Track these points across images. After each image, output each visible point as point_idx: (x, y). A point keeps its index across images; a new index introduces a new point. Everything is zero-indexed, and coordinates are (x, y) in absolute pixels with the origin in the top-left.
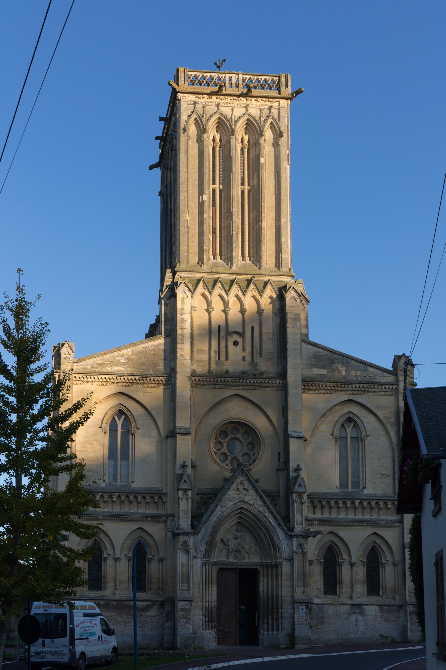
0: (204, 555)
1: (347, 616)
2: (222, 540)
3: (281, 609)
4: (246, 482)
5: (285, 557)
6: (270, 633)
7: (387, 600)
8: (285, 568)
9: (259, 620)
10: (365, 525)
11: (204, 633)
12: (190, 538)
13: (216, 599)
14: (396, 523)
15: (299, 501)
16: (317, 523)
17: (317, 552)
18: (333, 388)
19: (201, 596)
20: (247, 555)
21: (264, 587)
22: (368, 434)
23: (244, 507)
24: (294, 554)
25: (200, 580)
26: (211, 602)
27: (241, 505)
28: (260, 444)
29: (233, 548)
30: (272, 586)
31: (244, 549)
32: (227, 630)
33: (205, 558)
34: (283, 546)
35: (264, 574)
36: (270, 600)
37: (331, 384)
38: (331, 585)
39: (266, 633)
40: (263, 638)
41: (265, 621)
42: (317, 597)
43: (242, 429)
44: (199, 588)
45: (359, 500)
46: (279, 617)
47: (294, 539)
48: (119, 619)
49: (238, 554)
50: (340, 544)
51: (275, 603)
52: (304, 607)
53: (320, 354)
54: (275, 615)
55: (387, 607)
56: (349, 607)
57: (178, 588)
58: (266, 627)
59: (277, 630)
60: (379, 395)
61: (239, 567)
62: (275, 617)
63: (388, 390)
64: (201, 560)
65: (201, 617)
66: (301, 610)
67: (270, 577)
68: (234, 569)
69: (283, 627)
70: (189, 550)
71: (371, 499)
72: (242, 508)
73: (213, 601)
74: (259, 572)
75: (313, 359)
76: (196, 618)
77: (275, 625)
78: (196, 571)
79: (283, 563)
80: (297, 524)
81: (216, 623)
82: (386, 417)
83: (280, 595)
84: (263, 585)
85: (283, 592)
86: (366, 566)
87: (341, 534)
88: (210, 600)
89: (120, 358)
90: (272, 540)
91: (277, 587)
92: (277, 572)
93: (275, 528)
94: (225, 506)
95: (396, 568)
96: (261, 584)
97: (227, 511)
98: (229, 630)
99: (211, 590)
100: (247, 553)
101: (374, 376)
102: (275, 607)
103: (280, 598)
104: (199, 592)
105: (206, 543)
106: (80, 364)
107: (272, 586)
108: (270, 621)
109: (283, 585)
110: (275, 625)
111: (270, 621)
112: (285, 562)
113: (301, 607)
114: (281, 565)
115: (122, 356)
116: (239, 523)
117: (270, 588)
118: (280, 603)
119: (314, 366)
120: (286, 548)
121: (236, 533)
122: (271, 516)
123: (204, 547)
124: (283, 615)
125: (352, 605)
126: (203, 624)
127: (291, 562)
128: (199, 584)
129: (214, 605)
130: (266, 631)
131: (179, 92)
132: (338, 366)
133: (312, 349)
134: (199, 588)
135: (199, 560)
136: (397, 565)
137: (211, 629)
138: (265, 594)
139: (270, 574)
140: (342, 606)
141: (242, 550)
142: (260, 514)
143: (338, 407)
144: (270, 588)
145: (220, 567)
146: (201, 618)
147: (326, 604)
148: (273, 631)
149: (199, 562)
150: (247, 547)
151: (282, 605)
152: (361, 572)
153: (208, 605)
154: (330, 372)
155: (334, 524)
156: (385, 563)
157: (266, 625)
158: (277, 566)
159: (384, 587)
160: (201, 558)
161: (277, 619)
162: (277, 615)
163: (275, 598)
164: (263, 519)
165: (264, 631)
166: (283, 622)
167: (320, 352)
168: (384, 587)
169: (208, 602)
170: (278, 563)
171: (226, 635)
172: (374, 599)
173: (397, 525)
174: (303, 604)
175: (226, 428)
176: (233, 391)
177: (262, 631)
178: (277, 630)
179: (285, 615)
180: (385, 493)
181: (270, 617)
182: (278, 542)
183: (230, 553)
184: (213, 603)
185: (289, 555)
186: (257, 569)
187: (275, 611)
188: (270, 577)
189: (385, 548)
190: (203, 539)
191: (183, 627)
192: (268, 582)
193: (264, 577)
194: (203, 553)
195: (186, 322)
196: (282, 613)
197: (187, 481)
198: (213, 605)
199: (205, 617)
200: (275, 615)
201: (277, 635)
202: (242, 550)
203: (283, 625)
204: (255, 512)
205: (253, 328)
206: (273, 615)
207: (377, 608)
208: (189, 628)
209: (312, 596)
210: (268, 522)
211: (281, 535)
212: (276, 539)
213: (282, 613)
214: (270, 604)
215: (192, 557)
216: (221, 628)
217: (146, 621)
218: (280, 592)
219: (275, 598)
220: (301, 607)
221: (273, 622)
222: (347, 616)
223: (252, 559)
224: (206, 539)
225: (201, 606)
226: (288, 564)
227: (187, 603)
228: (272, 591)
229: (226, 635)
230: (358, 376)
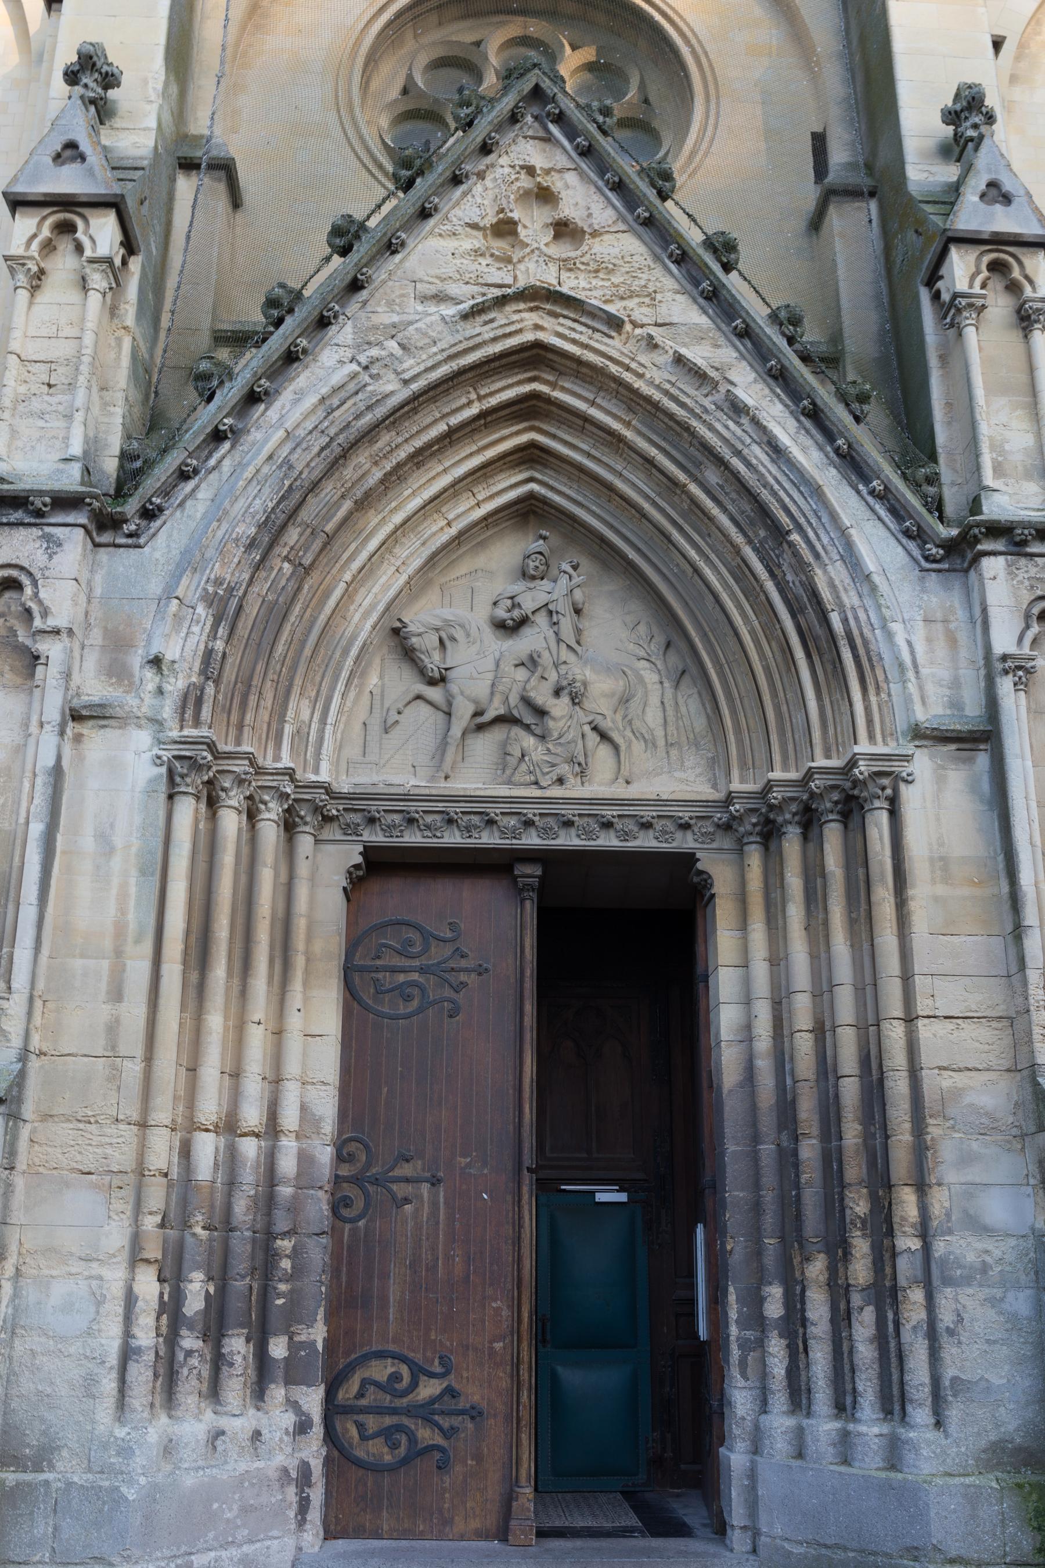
0: (191, 703)
2: (399, 640)
3: (921, 1187)
4: (571, 178)
5: (921, 715)
6: (824, 1427)
8: (936, 806)
9: (717, 1298)
11: (126, 1451)
12: (52, 545)
13: (326, 1105)
15: (999, 306)
19: (134, 1069)
20: (604, 752)
21: (747, 1001)
24: (1005, 686)
25: (138, 917)
26: (272, 1129)
27: (530, 325)
28: (687, 76)
29: (481, 689)
30: (823, 990)
31: (576, 700)
32: (429, 1389)
33: (197, 723)
34: (896, 627)
35: (742, 899)
36: (807, 1108)
39: (780, 1422)
40: (752, 1474)
41: (774, 1308)
43: (574, 48)
44: (117, 994)
46: (904, 1265)
47: (993, 567)
49: (529, 742)
51: (852, 1133)
54: (861, 1246)
58: (778, 1367)
59: (894, 1402)
61: (532, 840)
62: (860, 1271)
65: (115, 1276)
67: (795, 912)
68: (493, 865)
69: (949, 1372)
70: (45, 647)
72: (535, 356)
73: (290, 1118)
74: (706, 881)
76: (59, 1290)
77: (865, 1352)
78: (103, 838)
79: (903, 769)
80: (999, 470)
81: (318, 1334)
83: (896, 1058)
84: (746, 985)
85: (925, 1030)
88: (252, 1115)
90: (809, 605)
91: (868, 987)
92: (857, 858)
93: (817, 492)
96: (725, 983)
97: (411, 365)
98: (451, 1392)
99: (279, 1033)
100: (604, 736)
102: (854, 1170)
103: (898, 1086)
104: (113, 1029)
105: (209, 600)
107: (823, 990)
108: (818, 1308)
109: (920, 964)
110: (865, 1352)
111: (818, 1308)
112: (923, 764)
114: (890, 783)
116: (527, 512)
117: (802, 1005)
118: (902, 1135)
120: (920, 648)
121: (519, 587)
123: (198, 636)
124: (939, 1248)
126: (127, 1354)
127: (983, 760)
128: (118, 953)
129: (305, 1159)
130: (779, 1400)
134: (117, 994)
135: (142, 738)
137: (259, 1392)
138: (764, 1065)
139: (794, 882)
141: (559, 707)
142: (693, 394)
144: (802, 1005)
145: (376, 837)
146: (116, 1289)
148: (844, 1405)
149: (126, 765)
150: (602, 689)
151: (921, 1148)
153: (231, 1159)
157: (776, 1347)
158: (852, 800)
160: (157, 723)
161: (886, 1294)
162: (884, 1254)
163: (850, 1090)
164: (719, 431)
165: (764, 1406)
166: (946, 1318)
169: (229, 1126)
170: (863, 769)
171: (426, 1435)
177: (741, 1399)
178: (894, 1402)
179: (956, 1247)
181: (817, 1269)
182: (850, 599)
183: (456, 731)
184: (289, 1146)
185: (956, 704)
186: (688, 859)
187: (859, 1206)
188: (795, 912)
190: (189, 562)
192: (778, 960)
193: (743, 926)
194: (176, 685)
196: (924, 1233)
197: (85, 146)
198: (287, 1165)
199: (172, 1276)
200: (861, 1246)
201: (894, 1454)
202: (559, 707)
203: (950, 1352)
204: (652, 375)
206: (839, 1251)
210: (758, 454)
211: (878, 546)
212: (830, 577)
213: (924, 1233)
214: (809, 1150)
215: (53, 707)
216: (381, 1371)
218: (895, 1033)
219: (850, 1090)
221: (841, 1319)
223: (643, 764)
224: (218, 570)
225: (123, 1157)
226: (957, 778)
228: (823, 1030)
229: (426, 1435)
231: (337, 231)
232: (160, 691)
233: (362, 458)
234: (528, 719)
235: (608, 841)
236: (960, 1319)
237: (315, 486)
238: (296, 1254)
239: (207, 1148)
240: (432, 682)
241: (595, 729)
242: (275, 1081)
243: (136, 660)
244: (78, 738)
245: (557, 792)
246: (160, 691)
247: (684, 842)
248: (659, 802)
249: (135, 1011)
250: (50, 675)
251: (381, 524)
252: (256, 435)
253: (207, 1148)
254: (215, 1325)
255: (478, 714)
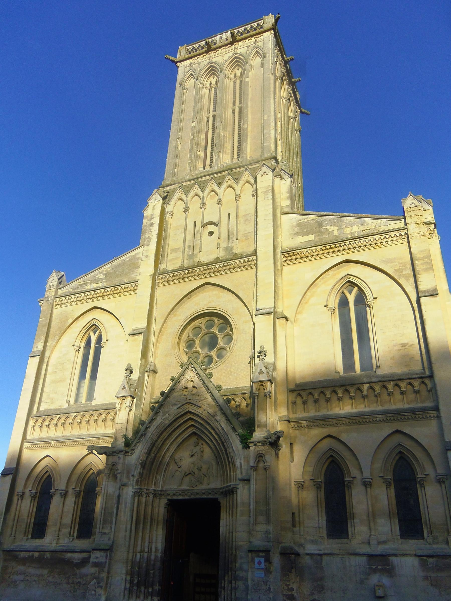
1: (363, 577)
7: (435, 546)
10: (380, 420)
14: (429, 412)
16: (305, 425)
17: (310, 469)
18: (322, 252)
19: (127, 543)
22: (374, 297)
23: (191, 411)
25: (129, 518)
37: (318, 248)
38: (338, 520)
42: (313, 542)
45: (368, 385)
48: (50, 579)
50: (346, 454)
52: (262, 560)
53: (305, 220)
55: (434, 559)
56: (365, 558)
57: (97, 530)
60: (384, 247)
63: (395, 238)
64: (133, 489)
65: (124, 577)
66: (257, 565)
71: (386, 381)
74: (219, 503)
75: (296, 228)
82: (396, 270)
86: (393, 486)
87: (344, 437)
89: (99, 275)
94: (167, 412)
95: (443, 486)
97: (170, 418)
101: (376, 228)
106: (64, 289)
113: (257, 560)
115: (101, 273)
119: (297, 234)
122: (224, 419)
125: (370, 556)
129: (156, 556)
131: (177, 62)
132: (327, 227)
133: (295, 218)
134: (126, 531)
135: (131, 488)
136: (444, 482)
140: (352, 557)
143: (331, 272)
145: (169, 498)
146: (124, 579)
147: (325, 554)
152: (384, 496)
154: (318, 235)
155: (331, 423)
156: (422, 480)
159: (428, 522)
160: (133, 485)
167: (305, 219)
168: (428, 522)
172: (412, 545)
173: (432, 415)
174: (261, 554)
175: (201, 324)
176: (202, 280)
180: (409, 370)
184: (153, 554)
186: (217, 499)
189: (419, 454)
191: (93, 592)
195: (155, 225)
198: (153, 557)
205: (229, 215)
207: (415, 561)
208: (100, 595)
209: (303, 541)
217: (79, 583)
220: (257, 560)
222: (363, 577)
227: (102, 554)
230: (353, 232)
231: (171, 379)
232: (133, 480)
233: (164, 434)
234: (193, 474)
235: (204, 497)
236: (238, 587)
237: (156, 441)
238: (154, 574)
239: (138, 555)
240: (179, 467)
241: (203, 474)
242: (150, 542)
243: (131, 475)
244: (123, 489)
245: (196, 488)
246: (133, 480)
247: (217, 496)
248: (211, 489)
249: (128, 534)
250: (118, 480)
251: (169, 443)
252: (148, 434)
253: (138, 555)
254: (138, 585)
255: (186, 473)
